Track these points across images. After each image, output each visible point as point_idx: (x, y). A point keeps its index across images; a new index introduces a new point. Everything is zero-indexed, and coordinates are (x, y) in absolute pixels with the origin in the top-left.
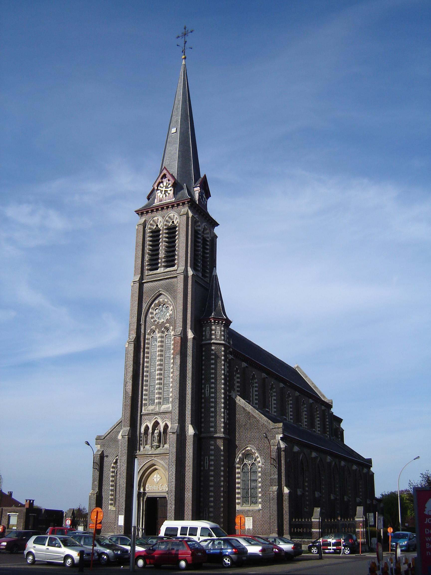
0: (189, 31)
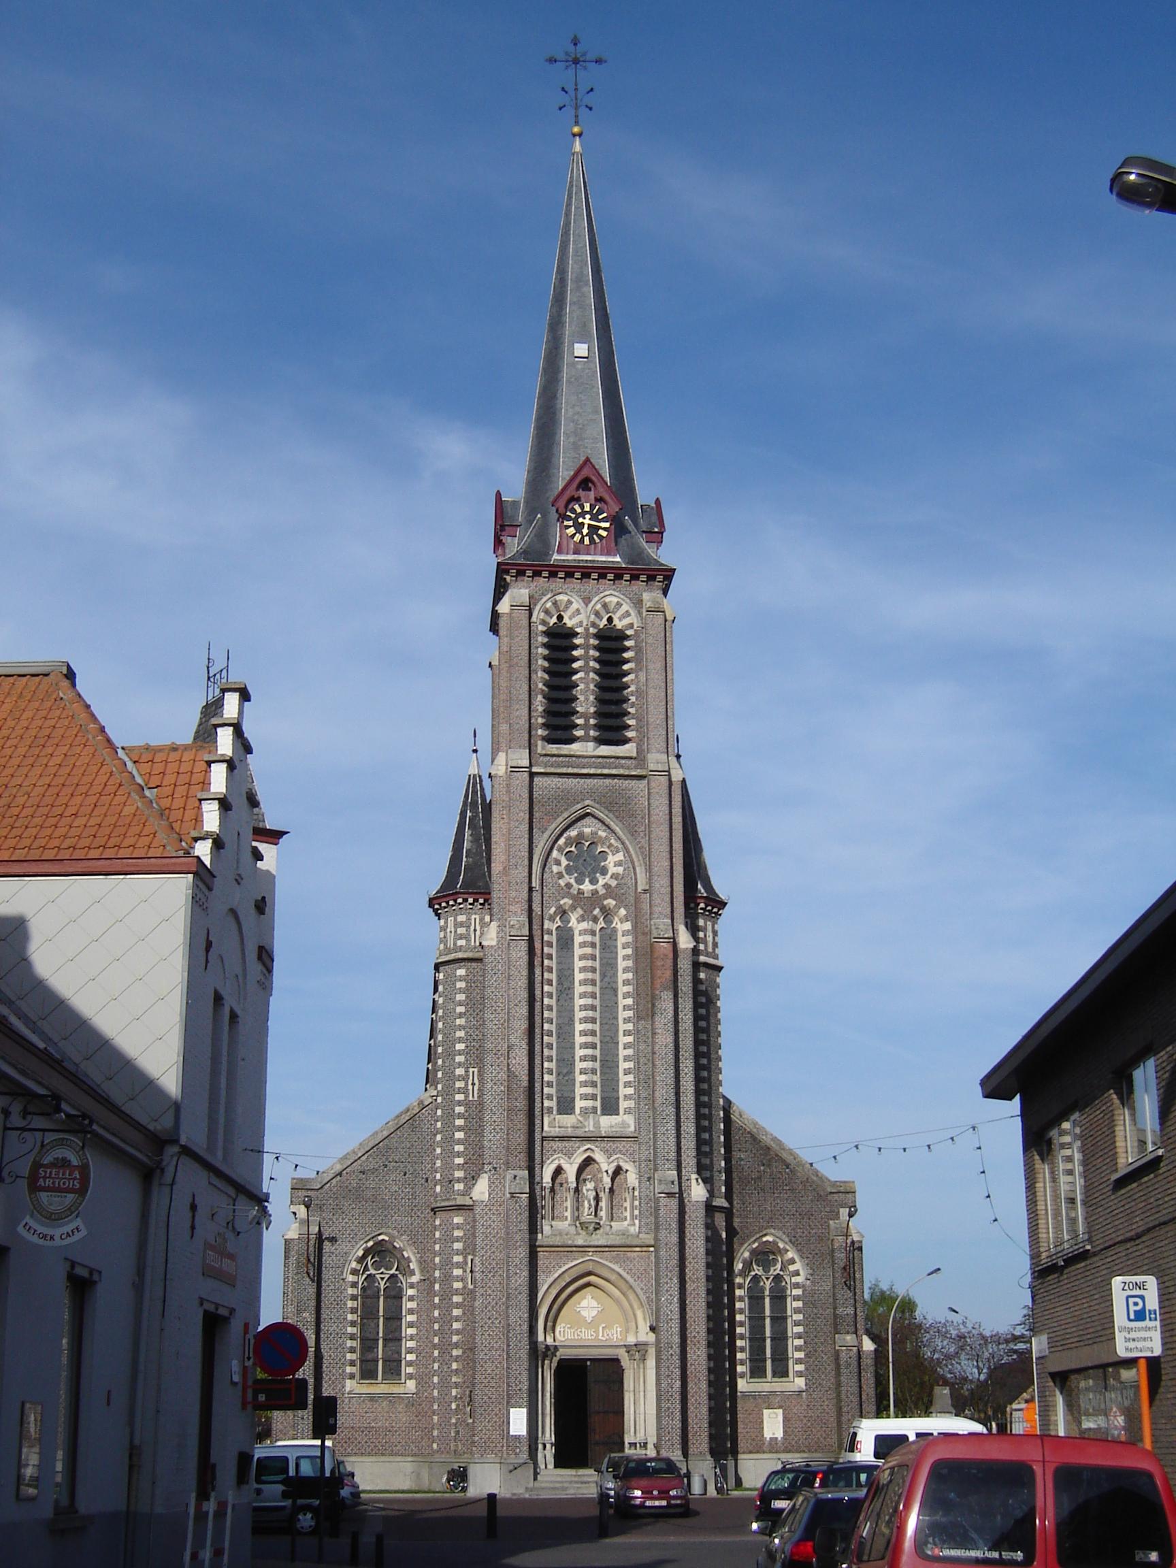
0: (571, 48)
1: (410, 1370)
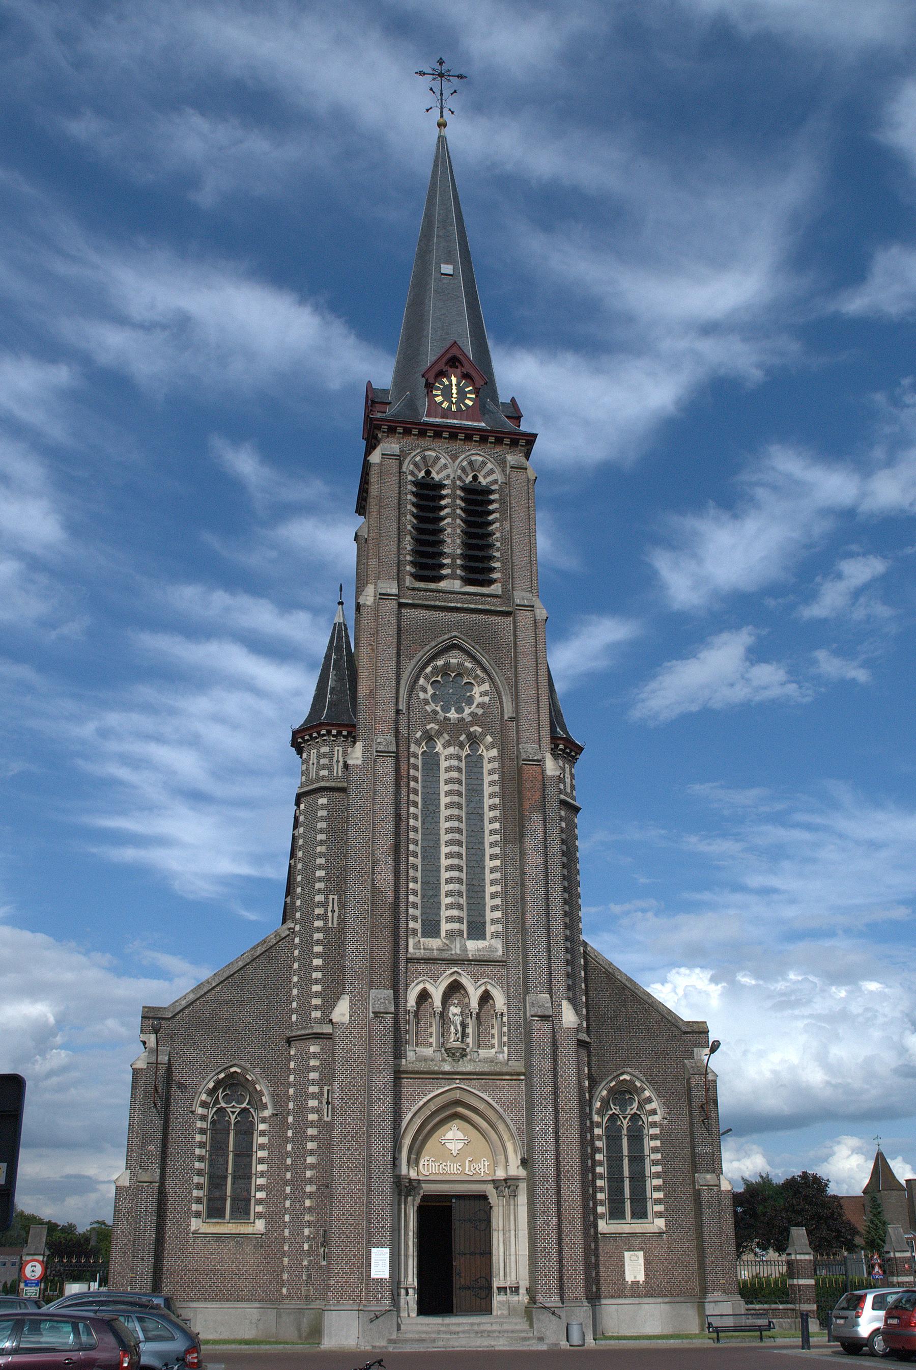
0: (437, 66)
1: (259, 1209)
